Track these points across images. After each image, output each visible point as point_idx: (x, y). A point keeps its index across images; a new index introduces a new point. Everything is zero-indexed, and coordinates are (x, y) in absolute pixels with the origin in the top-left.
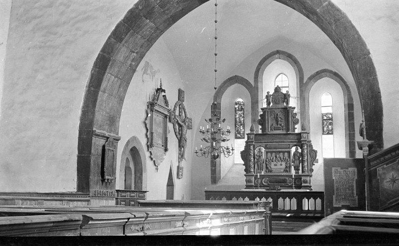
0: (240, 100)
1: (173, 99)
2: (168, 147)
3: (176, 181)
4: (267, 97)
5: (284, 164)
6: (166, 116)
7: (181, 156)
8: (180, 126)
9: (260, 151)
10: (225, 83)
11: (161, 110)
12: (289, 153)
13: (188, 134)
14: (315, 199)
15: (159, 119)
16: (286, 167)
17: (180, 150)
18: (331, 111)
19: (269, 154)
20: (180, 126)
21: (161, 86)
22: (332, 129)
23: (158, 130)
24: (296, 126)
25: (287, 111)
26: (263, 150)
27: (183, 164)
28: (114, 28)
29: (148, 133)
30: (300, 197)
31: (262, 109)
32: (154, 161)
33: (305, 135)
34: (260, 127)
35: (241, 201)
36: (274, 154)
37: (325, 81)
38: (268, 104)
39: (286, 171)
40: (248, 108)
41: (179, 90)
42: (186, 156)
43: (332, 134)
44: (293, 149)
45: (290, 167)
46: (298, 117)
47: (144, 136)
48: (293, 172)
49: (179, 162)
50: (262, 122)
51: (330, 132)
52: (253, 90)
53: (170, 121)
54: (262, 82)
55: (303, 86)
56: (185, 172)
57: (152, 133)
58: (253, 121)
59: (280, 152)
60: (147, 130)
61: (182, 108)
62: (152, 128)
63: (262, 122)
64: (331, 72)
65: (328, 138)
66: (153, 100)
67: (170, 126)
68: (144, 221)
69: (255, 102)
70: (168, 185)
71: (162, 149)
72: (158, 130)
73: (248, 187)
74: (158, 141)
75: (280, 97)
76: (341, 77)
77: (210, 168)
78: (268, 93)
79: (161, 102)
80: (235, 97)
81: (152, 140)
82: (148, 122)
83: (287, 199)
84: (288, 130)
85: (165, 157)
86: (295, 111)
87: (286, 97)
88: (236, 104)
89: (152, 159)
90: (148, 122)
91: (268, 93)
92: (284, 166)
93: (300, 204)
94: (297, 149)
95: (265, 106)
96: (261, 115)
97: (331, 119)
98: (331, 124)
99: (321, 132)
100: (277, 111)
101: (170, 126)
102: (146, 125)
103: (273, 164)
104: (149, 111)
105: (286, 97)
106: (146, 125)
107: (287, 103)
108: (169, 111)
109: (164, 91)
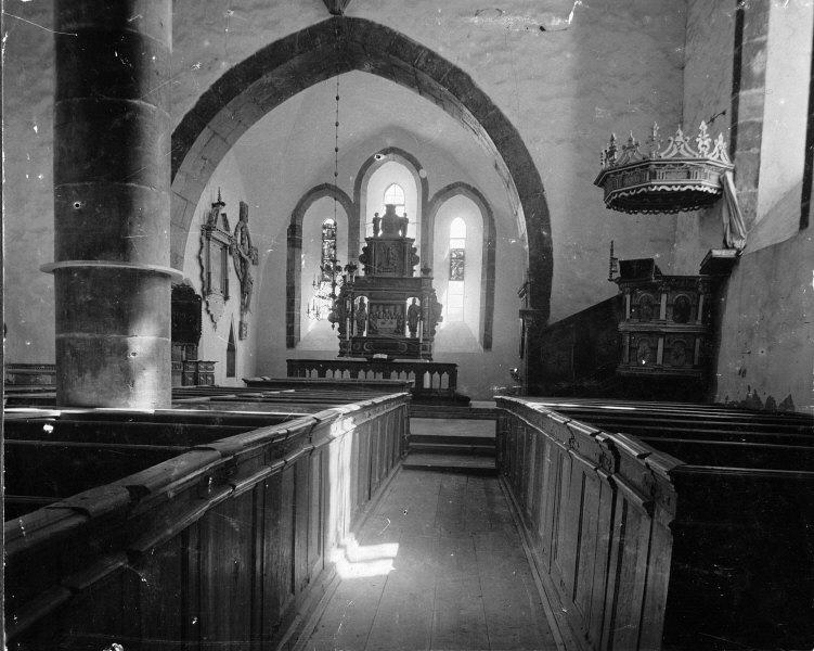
0: (330, 222)
1: (233, 220)
2: (230, 294)
3: (240, 346)
4: (376, 221)
5: (395, 321)
6: (225, 246)
7: (244, 307)
8: (243, 261)
9: (362, 300)
10: (309, 194)
11: (221, 238)
12: (404, 306)
13: (252, 271)
14: (441, 374)
15: (215, 250)
16: (398, 327)
17: (243, 297)
18: (463, 247)
19: (374, 307)
20: (243, 261)
21: (219, 199)
22: (463, 273)
23: (216, 268)
24: (415, 268)
25: (403, 243)
26: (366, 300)
27: (247, 318)
28: (180, 121)
29: (204, 274)
30: (420, 370)
31: (367, 240)
32: (212, 316)
33: (426, 282)
34: (362, 266)
35: (603, 417)
36: (381, 308)
37: (460, 200)
38: (376, 230)
39: (397, 332)
40: (343, 234)
41: (242, 204)
42: (252, 305)
43: (463, 279)
44: (409, 301)
45: (404, 326)
46: (418, 254)
47: (198, 278)
48: (408, 334)
49: (242, 315)
50: (366, 258)
51: (460, 277)
52: (354, 209)
53: (230, 253)
54: (366, 196)
55: (428, 207)
56: (249, 331)
57: (209, 274)
58: (352, 255)
59: (390, 305)
60: (202, 268)
61: (245, 235)
62: (209, 267)
63: (366, 258)
64: (468, 187)
65: (456, 287)
66: (209, 222)
67: (230, 260)
68: (597, 434)
69: (354, 228)
70: (228, 350)
71: (220, 297)
72: (216, 268)
73: (342, 354)
74: (216, 284)
75: (392, 222)
76: (416, 161)
77: (285, 325)
78: (377, 214)
79: (220, 225)
80: (325, 215)
81: (209, 283)
82: (203, 256)
83: (436, 375)
84: (403, 272)
85: (225, 308)
86: (415, 245)
87: (403, 223)
88: (325, 228)
89: (208, 312)
90: (203, 256)
91: (377, 214)
92: (394, 326)
93: (420, 380)
94: (414, 301)
95: (370, 234)
96: (364, 249)
97: (463, 258)
98: (462, 265)
99: (448, 275)
100: (388, 243)
101: (230, 260)
102: (200, 261)
103: (379, 321)
104: (204, 238)
105: (403, 223)
106: (200, 261)
107: (404, 232)
108: (230, 238)
109: (223, 204)
